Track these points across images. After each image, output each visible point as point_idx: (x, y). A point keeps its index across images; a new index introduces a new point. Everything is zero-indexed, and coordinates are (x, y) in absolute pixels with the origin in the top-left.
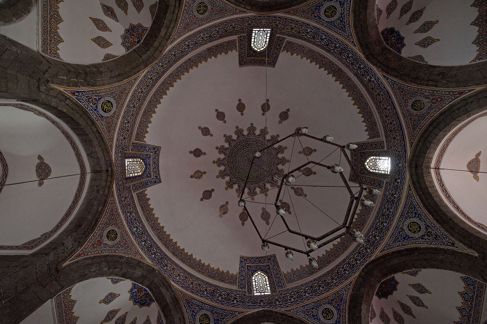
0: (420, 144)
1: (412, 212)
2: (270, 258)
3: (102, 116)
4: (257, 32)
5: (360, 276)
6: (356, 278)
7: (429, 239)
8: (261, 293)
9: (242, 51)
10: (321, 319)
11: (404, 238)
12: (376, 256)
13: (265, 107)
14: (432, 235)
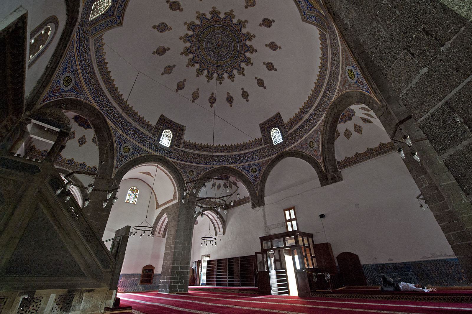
0: (172, 166)
1: (135, 150)
3: (353, 67)
4: (280, 140)
5: (95, 109)
9: (282, 124)
11: (120, 143)
13: (245, 95)
14: (121, 158)
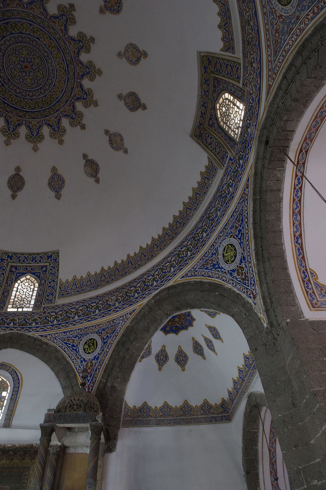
2: (51, 255)
6: (142, 306)
7: (237, 278)
8: (18, 308)
10: (80, 351)
12: (175, 281)
